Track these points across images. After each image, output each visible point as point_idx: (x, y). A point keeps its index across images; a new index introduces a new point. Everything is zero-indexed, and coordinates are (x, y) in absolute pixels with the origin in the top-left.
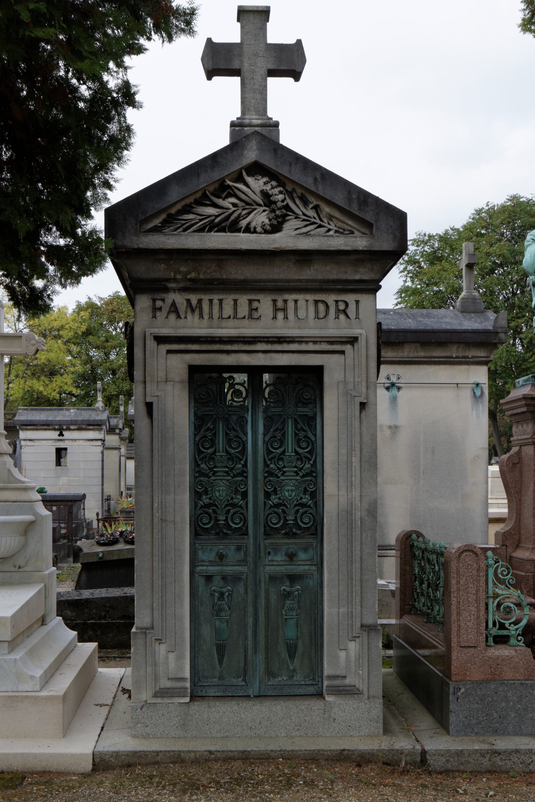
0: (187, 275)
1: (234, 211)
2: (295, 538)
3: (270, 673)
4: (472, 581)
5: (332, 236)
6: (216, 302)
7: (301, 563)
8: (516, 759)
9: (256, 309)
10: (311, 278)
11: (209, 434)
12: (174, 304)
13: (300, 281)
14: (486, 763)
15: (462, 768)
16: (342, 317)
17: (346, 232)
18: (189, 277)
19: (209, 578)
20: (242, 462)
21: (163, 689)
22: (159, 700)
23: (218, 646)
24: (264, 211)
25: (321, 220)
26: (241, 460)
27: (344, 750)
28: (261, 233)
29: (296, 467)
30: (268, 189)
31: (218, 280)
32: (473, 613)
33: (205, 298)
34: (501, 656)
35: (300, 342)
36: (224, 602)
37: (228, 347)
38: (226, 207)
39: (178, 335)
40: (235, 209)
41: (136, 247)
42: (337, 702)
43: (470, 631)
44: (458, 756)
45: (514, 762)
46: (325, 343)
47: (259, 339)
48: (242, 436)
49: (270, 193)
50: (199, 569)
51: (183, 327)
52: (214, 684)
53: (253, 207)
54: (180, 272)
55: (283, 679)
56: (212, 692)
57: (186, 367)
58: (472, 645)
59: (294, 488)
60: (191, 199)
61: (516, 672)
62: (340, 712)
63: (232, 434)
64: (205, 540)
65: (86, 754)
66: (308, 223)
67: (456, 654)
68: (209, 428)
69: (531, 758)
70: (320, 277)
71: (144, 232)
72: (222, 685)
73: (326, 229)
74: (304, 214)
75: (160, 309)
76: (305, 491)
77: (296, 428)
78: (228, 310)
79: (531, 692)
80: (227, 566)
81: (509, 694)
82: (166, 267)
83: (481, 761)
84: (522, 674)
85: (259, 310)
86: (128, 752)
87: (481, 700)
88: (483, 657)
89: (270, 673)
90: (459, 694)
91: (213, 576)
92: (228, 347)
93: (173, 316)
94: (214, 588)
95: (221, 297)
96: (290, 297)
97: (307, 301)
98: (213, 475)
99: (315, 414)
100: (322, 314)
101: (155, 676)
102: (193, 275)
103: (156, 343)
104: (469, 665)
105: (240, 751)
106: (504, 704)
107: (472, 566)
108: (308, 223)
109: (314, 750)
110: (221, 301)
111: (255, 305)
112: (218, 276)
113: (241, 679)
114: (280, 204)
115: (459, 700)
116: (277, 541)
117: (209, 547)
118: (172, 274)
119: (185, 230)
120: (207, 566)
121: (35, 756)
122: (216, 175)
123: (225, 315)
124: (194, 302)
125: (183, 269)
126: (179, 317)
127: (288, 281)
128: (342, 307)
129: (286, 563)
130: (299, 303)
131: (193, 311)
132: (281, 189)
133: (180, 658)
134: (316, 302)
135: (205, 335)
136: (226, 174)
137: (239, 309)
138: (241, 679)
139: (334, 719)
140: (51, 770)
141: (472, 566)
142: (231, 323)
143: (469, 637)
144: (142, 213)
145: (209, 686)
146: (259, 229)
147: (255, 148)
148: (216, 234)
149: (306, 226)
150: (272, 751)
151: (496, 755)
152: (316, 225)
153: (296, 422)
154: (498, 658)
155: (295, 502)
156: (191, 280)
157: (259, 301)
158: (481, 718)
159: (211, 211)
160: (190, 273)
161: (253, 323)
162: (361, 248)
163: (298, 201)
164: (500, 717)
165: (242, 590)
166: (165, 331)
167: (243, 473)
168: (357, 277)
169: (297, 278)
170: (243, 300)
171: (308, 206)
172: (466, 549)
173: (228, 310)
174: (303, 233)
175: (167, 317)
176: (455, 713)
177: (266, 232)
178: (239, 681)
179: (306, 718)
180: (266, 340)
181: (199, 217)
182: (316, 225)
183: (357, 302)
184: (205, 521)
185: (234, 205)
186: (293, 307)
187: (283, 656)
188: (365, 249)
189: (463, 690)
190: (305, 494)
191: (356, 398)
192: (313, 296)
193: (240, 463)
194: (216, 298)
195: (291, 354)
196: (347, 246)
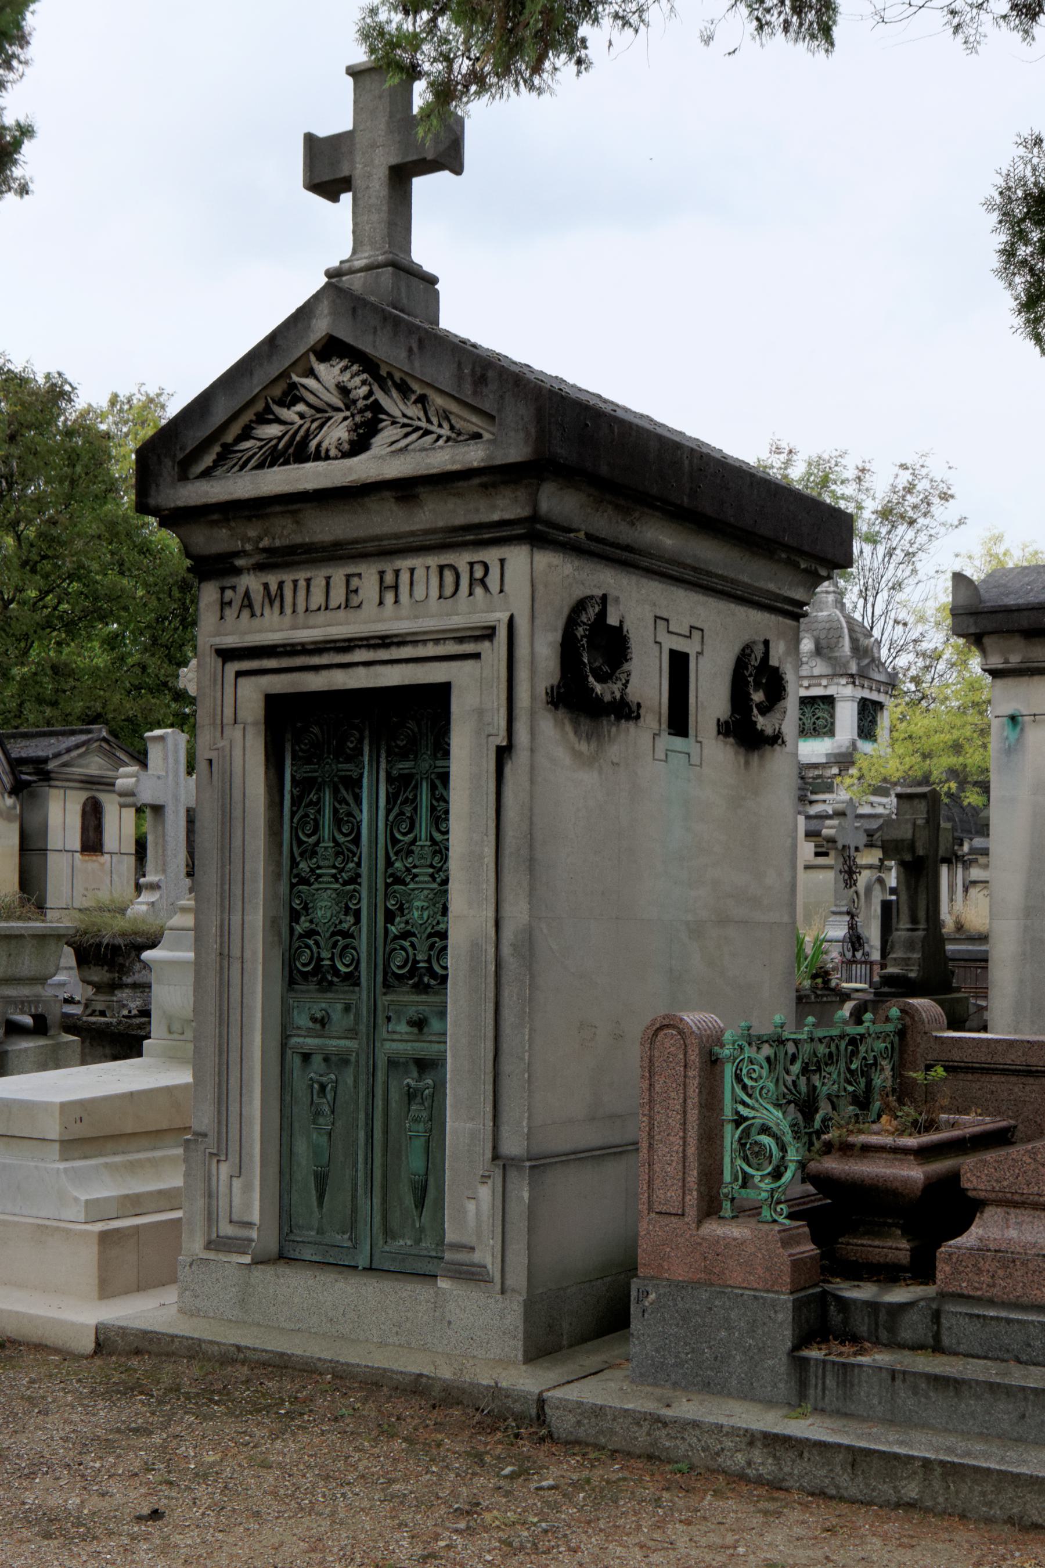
0: (258, 542)
1: (301, 426)
2: (427, 993)
3: (388, 1233)
4: (674, 1085)
5: (441, 448)
6: (302, 584)
7: (434, 1038)
8: (695, 1440)
9: (356, 591)
10: (428, 526)
11: (312, 811)
12: (247, 594)
13: (413, 534)
14: (642, 1437)
15: (603, 1440)
16: (479, 591)
17: (462, 438)
18: (261, 545)
19: (306, 1057)
20: (356, 859)
21: (222, 1237)
22: (211, 1255)
23: (316, 1175)
24: (345, 419)
25: (429, 421)
26: (354, 855)
27: (421, 1375)
28: (336, 458)
29: (334, 867)
30: (345, 379)
31: (301, 545)
32: (675, 1149)
33: (288, 577)
34: (724, 1238)
35: (415, 643)
36: (325, 1101)
37: (316, 660)
38: (289, 420)
39: (246, 644)
40: (301, 422)
41: (172, 505)
42: (455, 1292)
43: (669, 1183)
44: (596, 1416)
45: (690, 1445)
46: (452, 642)
47: (357, 643)
48: (356, 812)
49: (350, 385)
50: (294, 1040)
51: (260, 631)
52: (310, 1239)
53: (327, 415)
54: (249, 539)
55: (404, 1243)
56: (308, 1254)
57: (262, 698)
58: (674, 1212)
59: (426, 904)
60: (249, 416)
61: (750, 1273)
62: (458, 1311)
63: (343, 809)
64: (302, 992)
65: (87, 1325)
66: (409, 429)
67: (645, 1226)
68: (311, 800)
69: (721, 1442)
70: (441, 524)
71: (197, 478)
72: (319, 1244)
73: (434, 436)
74: (404, 416)
75: (230, 603)
76: (347, 909)
77: (433, 795)
78: (318, 598)
79: (773, 1315)
80: (330, 1038)
81: (733, 1315)
82: (229, 533)
83: (635, 1432)
84: (759, 1277)
85: (360, 591)
86: (137, 1330)
87: (683, 1319)
88: (691, 1236)
89: (388, 1233)
90: (647, 1304)
91: (311, 1054)
92: (316, 660)
93: (246, 614)
94: (312, 1075)
95: (308, 575)
96: (404, 564)
97: (428, 568)
98: (316, 880)
99: (361, 775)
100: (449, 590)
101: (210, 1213)
102: (265, 543)
103: (220, 661)
104: (668, 1250)
105: (277, 1353)
106: (723, 1334)
107: (675, 1056)
108: (409, 429)
109: (378, 1368)
110: (308, 581)
111: (355, 582)
112: (298, 539)
113: (346, 1236)
114: (361, 404)
115: (646, 1315)
116: (402, 998)
117: (308, 1005)
118: (239, 543)
119: (242, 468)
120: (305, 1037)
121: (31, 1318)
122: (274, 370)
123: (314, 606)
124: (274, 588)
125: (252, 533)
126: (253, 615)
127: (397, 536)
128: (479, 573)
129: (411, 1038)
130: (416, 572)
131: (271, 603)
132: (365, 376)
133: (247, 1188)
134: (441, 568)
135: (280, 642)
136: (287, 365)
137: (332, 593)
138: (346, 1236)
139: (450, 1323)
140: (48, 1343)
141: (675, 1056)
142: (322, 617)
143: (669, 1194)
144: (181, 449)
145: (303, 1242)
146: (333, 452)
147: (326, 312)
148: (282, 468)
149: (406, 435)
150: (319, 1359)
151: (660, 1425)
152: (421, 432)
153: (336, 791)
154: (718, 1242)
155: (429, 930)
156: (265, 550)
157: (359, 575)
158: (683, 1356)
159: (273, 430)
160: (261, 539)
161: (351, 614)
162: (475, 464)
163: (395, 393)
164: (716, 1358)
165: (350, 1081)
166: (230, 641)
167: (355, 879)
168: (496, 517)
169: (408, 529)
170: (338, 575)
171: (408, 399)
172: (665, 1022)
173: (318, 598)
174: (401, 450)
175: (238, 617)
176: (638, 1338)
177: (345, 455)
178: (344, 1240)
179: (409, 1314)
180: (365, 643)
181: (259, 444)
182: (421, 432)
183: (502, 561)
184: (304, 959)
185: (302, 416)
186: (408, 581)
187: (407, 1202)
188: (482, 464)
189: (653, 1296)
190: (346, 914)
191: (491, 738)
192: (436, 558)
193: (352, 861)
194: (301, 576)
195: (404, 665)
196: (453, 463)
